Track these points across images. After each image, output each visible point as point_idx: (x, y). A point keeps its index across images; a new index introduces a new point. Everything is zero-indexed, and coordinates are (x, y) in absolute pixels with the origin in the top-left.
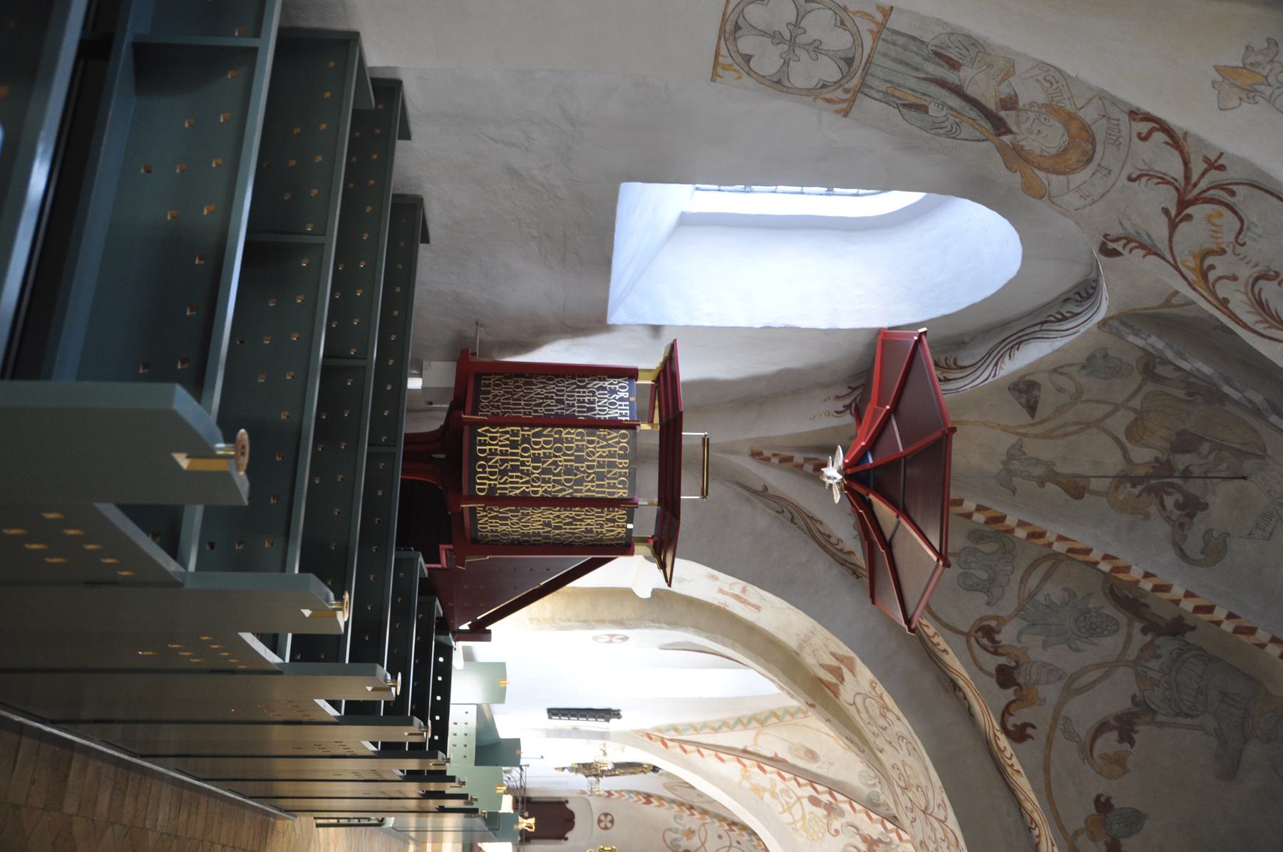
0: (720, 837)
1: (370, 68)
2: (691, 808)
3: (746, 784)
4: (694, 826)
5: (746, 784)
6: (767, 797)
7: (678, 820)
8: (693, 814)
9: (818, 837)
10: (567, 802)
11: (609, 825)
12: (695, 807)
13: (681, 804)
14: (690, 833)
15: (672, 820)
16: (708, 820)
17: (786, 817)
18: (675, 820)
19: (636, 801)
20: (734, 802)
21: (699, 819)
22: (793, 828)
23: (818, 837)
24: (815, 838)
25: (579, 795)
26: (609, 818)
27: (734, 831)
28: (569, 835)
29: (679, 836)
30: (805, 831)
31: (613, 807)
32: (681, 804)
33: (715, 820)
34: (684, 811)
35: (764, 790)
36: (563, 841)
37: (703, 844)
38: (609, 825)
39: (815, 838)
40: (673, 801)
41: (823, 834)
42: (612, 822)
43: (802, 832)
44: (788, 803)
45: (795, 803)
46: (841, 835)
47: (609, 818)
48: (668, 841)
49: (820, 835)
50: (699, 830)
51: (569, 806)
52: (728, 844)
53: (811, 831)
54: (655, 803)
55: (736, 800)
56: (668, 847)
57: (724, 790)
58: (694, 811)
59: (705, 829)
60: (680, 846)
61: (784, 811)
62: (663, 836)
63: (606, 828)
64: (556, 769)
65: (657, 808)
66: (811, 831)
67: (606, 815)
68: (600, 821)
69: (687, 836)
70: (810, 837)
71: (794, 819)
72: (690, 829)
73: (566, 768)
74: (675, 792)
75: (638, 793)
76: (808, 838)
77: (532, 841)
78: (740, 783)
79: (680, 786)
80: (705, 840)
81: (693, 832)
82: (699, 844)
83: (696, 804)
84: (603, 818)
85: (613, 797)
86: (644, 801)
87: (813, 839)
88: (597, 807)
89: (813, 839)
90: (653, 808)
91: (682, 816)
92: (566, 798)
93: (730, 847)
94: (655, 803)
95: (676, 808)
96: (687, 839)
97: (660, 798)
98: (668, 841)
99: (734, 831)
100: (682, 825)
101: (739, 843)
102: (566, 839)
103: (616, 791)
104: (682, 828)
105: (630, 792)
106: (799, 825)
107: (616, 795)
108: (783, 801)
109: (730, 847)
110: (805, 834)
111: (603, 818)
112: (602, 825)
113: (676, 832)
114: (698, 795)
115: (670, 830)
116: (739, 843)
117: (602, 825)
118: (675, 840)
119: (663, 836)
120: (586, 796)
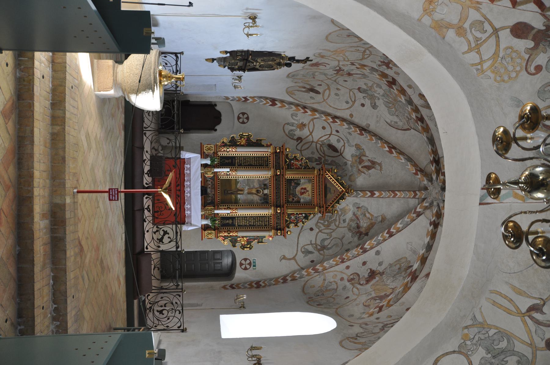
0: (324, 128)
1: (152, 15)
2: (304, 107)
3: (427, 20)
4: (306, 121)
5: (427, 20)
6: (451, 34)
7: (294, 117)
8: (306, 112)
9: (510, 78)
10: (216, 105)
11: (245, 121)
12: (307, 107)
13: (297, 105)
14: (302, 126)
15: (290, 117)
16: (317, 115)
17: (473, 57)
18: (292, 117)
19: (265, 104)
20: (413, 40)
21: (310, 115)
22: (477, 70)
23: (510, 78)
24: (506, 78)
25: (224, 100)
26: (246, 116)
27: (337, 122)
28: (217, 127)
29: (295, 128)
30: (493, 72)
31: (248, 108)
32: (297, 105)
33: (322, 115)
34: (300, 110)
35: (449, 26)
36: (213, 132)
37: (311, 133)
38: (245, 121)
39: (506, 78)
40: (291, 103)
41: (518, 73)
42: (248, 118)
43: (489, 73)
44: (477, 39)
45: (489, 37)
46: (544, 72)
47: (246, 116)
48: (287, 132)
49: (514, 75)
50: (309, 123)
51: (218, 108)
52: (329, 133)
53: (502, 71)
54: (279, 104)
55: (415, 38)
56: (287, 135)
57: (400, 27)
58: (307, 110)
59: (313, 123)
60: (295, 135)
61: (470, 50)
62: (283, 128)
63: (243, 123)
64: (207, 60)
65: (280, 109)
66: (502, 71)
67: (243, 114)
68: (239, 118)
69: (300, 128)
70: (498, 78)
71: (481, 58)
72: (302, 123)
73: (215, 59)
74: (294, 97)
75: (266, 98)
76: (495, 80)
77: (191, 131)
78: (419, 20)
79: (298, 91)
80: (313, 131)
81: (305, 125)
82: (309, 133)
83: (308, 105)
84: (241, 116)
85: (248, 101)
86: (271, 103)
87: (503, 81)
88: (237, 108)
89: (503, 81)
90: (276, 110)
91: (297, 114)
92: (215, 102)
93: (330, 135)
94: (279, 104)
95: (294, 108)
96: (300, 130)
97: (282, 101)
98: (287, 132)
99: (337, 122)
100: (297, 120)
101: (337, 131)
102: (216, 130)
103: (251, 97)
104: (297, 123)
105: (261, 97)
106: (486, 66)
107: (251, 100)
108: (471, 38)
109: (330, 135)
110: (492, 75)
111: (241, 116)
112: (241, 120)
113: (293, 126)
114: (364, 44)
115: (288, 124)
116: (337, 131)
117: (241, 120)
118: (292, 130)
119: (283, 128)
120: (229, 101)
